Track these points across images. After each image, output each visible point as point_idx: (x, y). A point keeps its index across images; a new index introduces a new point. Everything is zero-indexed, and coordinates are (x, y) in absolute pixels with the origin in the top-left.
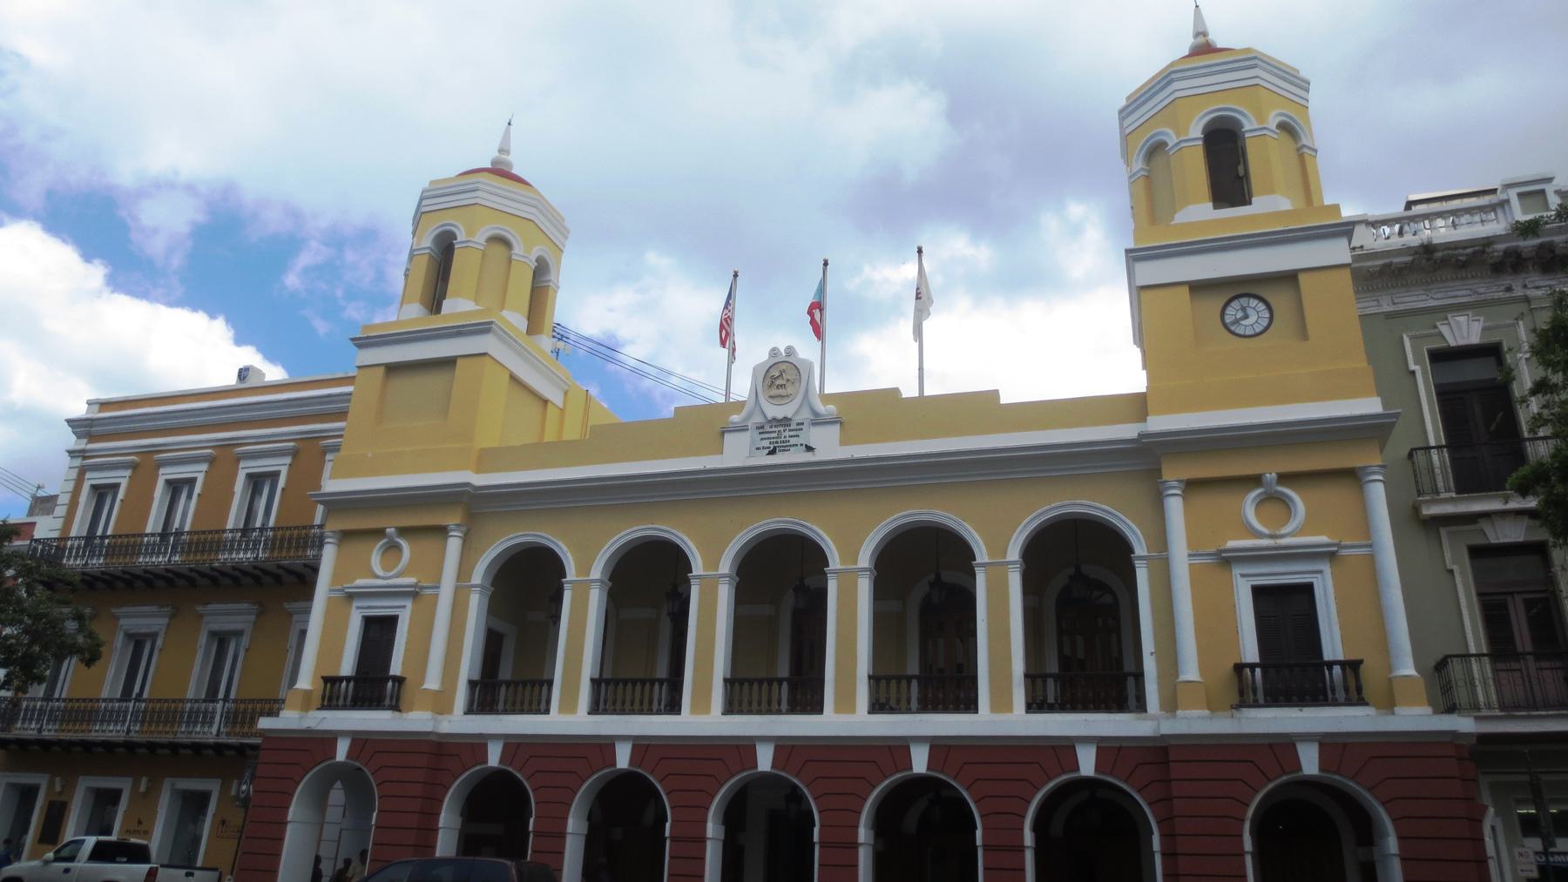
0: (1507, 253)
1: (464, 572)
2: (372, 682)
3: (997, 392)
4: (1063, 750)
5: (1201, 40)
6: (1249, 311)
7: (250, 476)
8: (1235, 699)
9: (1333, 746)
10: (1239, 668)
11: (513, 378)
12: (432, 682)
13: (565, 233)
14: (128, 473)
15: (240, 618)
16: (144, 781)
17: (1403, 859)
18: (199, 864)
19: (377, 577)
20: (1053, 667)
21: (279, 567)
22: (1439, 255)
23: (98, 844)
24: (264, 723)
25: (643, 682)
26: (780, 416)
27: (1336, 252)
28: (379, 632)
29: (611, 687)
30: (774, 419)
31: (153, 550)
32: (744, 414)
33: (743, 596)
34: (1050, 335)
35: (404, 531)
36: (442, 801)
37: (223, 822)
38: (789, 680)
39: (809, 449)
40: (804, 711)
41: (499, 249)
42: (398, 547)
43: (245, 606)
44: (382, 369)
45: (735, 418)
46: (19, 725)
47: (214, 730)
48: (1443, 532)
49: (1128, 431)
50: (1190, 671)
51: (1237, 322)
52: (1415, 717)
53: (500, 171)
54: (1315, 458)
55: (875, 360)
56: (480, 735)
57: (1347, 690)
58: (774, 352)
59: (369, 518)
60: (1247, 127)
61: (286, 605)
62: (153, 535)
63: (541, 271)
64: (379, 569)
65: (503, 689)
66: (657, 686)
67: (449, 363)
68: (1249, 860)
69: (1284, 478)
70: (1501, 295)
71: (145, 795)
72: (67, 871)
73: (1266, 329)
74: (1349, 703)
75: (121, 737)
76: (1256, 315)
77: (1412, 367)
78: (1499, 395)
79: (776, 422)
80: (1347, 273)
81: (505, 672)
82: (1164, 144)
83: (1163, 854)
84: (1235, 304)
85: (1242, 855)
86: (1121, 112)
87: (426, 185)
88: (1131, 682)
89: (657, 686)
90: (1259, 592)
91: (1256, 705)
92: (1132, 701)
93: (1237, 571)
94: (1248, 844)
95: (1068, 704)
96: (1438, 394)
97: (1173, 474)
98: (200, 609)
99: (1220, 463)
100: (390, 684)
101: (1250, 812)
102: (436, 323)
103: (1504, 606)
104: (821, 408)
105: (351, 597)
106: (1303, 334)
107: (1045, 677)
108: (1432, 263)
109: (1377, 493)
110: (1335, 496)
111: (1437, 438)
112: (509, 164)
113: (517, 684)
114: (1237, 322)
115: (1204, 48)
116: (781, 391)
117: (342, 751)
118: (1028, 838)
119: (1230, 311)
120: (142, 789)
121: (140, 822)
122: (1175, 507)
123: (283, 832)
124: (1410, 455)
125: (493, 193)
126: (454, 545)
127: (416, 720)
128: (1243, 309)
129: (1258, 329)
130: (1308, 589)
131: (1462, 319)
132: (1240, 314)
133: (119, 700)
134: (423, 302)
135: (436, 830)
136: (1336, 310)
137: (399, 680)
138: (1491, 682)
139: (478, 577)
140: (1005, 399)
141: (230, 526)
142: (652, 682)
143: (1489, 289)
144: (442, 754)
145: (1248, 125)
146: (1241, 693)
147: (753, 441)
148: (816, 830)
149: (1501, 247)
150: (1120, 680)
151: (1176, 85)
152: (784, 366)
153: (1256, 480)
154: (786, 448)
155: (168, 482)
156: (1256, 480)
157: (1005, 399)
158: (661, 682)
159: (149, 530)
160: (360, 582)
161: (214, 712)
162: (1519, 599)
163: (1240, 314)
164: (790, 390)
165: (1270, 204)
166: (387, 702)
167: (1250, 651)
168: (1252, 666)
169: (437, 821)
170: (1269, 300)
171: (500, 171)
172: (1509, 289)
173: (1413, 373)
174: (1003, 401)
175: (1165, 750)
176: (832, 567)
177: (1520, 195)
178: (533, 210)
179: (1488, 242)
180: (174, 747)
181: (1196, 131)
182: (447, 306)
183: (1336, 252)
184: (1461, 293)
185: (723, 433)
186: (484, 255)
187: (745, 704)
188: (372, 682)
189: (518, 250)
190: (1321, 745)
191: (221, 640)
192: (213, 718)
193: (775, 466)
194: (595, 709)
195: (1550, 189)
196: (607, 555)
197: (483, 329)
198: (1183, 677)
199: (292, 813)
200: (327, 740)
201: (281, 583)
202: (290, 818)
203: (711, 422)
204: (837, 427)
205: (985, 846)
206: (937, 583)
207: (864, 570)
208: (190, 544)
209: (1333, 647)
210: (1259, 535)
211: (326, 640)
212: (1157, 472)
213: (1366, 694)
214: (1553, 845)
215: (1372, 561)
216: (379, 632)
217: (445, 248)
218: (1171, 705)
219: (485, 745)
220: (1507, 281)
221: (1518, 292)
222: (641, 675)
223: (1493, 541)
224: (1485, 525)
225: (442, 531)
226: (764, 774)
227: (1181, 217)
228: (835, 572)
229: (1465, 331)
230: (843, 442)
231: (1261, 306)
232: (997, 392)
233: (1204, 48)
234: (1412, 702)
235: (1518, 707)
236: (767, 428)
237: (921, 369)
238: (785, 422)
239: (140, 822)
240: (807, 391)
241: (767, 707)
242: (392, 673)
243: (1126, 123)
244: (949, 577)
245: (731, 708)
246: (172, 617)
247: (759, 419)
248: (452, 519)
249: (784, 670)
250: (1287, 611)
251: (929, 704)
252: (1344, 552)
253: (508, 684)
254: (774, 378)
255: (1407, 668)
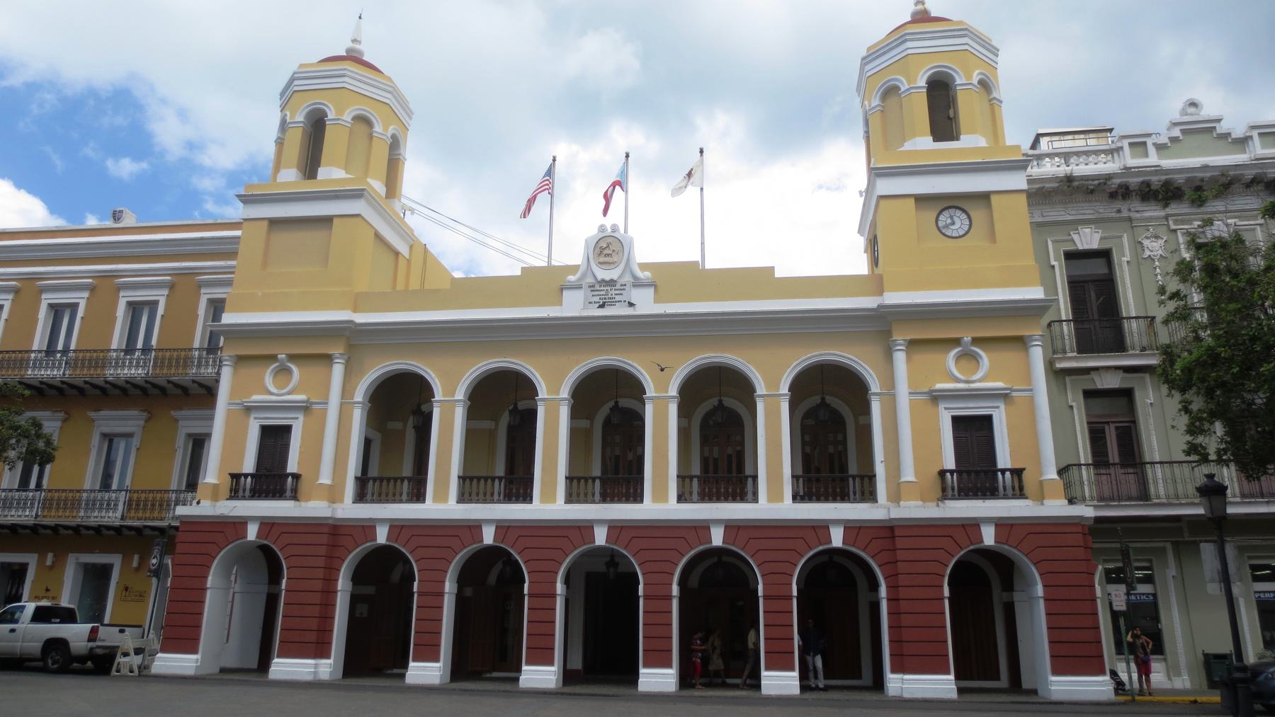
0: (1120, 186)
1: (346, 392)
2: (271, 477)
3: (773, 268)
4: (821, 528)
5: (920, 7)
6: (956, 219)
7: (130, 304)
8: (940, 494)
9: (1004, 526)
10: (942, 473)
11: (377, 235)
12: (325, 479)
13: (410, 114)
14: (10, 297)
15: (131, 423)
16: (50, 557)
17: (1046, 600)
18: (106, 621)
19: (272, 394)
20: (696, 470)
21: (169, 382)
22: (1076, 184)
23: (38, 609)
24: (181, 511)
25: (486, 479)
26: (607, 279)
27: (1017, 181)
28: (275, 438)
29: (377, 483)
30: (603, 280)
31: (38, 364)
32: (578, 275)
33: (575, 414)
34: (789, 220)
35: (292, 358)
36: (339, 570)
37: (126, 589)
38: (600, 478)
39: (631, 305)
40: (517, 501)
41: (362, 128)
42: (289, 371)
43: (135, 413)
44: (266, 223)
45: (572, 278)
46: (82, 514)
47: (119, 514)
48: (1068, 379)
49: (869, 302)
50: (908, 475)
51: (947, 226)
52: (1056, 507)
53: (353, 57)
54: (997, 327)
55: (662, 232)
56: (370, 519)
57: (1013, 488)
58: (602, 228)
59: (263, 347)
60: (958, 81)
61: (173, 413)
62: (40, 351)
63: (395, 145)
64: (275, 390)
65: (371, 482)
66: (497, 482)
67: (326, 221)
68: (947, 602)
69: (977, 341)
70: (1113, 215)
71: (51, 568)
72: (13, 631)
73: (967, 233)
74: (1014, 497)
75: (31, 522)
76: (959, 223)
77: (1053, 263)
78: (1107, 285)
79: (604, 282)
80: (1023, 197)
81: (373, 472)
82: (898, 88)
83: (889, 600)
84: (946, 213)
85: (942, 599)
86: (863, 59)
87: (295, 68)
88: (750, 481)
89: (497, 482)
90: (956, 420)
91: (953, 498)
92: (750, 495)
93: (942, 406)
94: (946, 592)
95: (707, 496)
96: (1069, 283)
97: (900, 337)
98: (92, 414)
99: (935, 329)
100: (290, 479)
101: (948, 572)
102: (309, 186)
103: (1103, 431)
104: (640, 274)
105: (249, 410)
106: (992, 236)
107: (691, 478)
108: (1072, 189)
109: (1037, 355)
110: (1009, 357)
111: (1067, 314)
112: (361, 53)
113: (381, 479)
114: (947, 226)
115: (922, 17)
116: (607, 259)
117: (252, 532)
118: (675, 590)
119: (941, 217)
120: (49, 563)
121: (47, 590)
122: (900, 358)
123: (204, 596)
124: (1049, 325)
125: (353, 78)
126: (338, 370)
127: (312, 508)
128: (951, 217)
129: (961, 233)
130: (989, 419)
131: (1087, 230)
132: (949, 221)
133: (18, 490)
134: (299, 169)
135: (335, 592)
136: (1014, 218)
137: (296, 477)
138: (1151, 481)
139: (359, 396)
140: (778, 274)
141: (114, 346)
142: (493, 479)
143: (1106, 209)
144: (336, 534)
145: (959, 80)
146: (944, 490)
147: (586, 298)
148: (641, 587)
149: (1117, 181)
150: (742, 480)
151: (909, 44)
152: (610, 240)
153: (956, 342)
154: (613, 303)
155: (51, 306)
156: (956, 342)
157: (778, 274)
158: (500, 479)
159: (35, 347)
160: (255, 397)
161: (117, 500)
162: (1112, 426)
163: (949, 221)
164: (615, 258)
165: (971, 141)
166: (288, 493)
167: (950, 462)
168: (952, 472)
169: (336, 586)
170: (972, 214)
171: (353, 57)
172: (1119, 211)
173: (1053, 267)
174: (777, 275)
175: (892, 529)
176: (648, 395)
177: (1131, 144)
178: (389, 95)
179: (1109, 177)
180: (77, 529)
181: (922, 82)
182: (322, 173)
183: (1017, 181)
184: (1088, 210)
185: (562, 290)
186: (351, 132)
187: (582, 495)
188: (271, 477)
189: (378, 128)
190: (996, 525)
191: (110, 438)
192: (116, 505)
193: (606, 317)
194: (461, 500)
195: (1150, 142)
196: (468, 382)
197: (357, 194)
198: (903, 479)
199: (210, 581)
200: (239, 525)
201: (176, 396)
202: (209, 585)
203: (548, 281)
204: (652, 290)
205: (765, 597)
206: (514, 412)
207: (673, 397)
208: (76, 360)
209: (1004, 459)
210: (958, 380)
211: (230, 445)
212: (888, 333)
213: (1027, 490)
214: (1134, 589)
215: (1031, 400)
216: (275, 438)
217: (317, 126)
218: (895, 497)
219: (374, 527)
220: (1118, 204)
221: (1125, 214)
222: (582, 475)
223: (1099, 387)
224: (1094, 375)
225: (328, 359)
226: (600, 548)
227: (908, 146)
228: (650, 398)
229: (1088, 239)
230: (656, 301)
231: (964, 216)
232: (773, 268)
233: (922, 17)
234: (1053, 497)
235: (1112, 499)
236: (597, 287)
237: (703, 243)
238: (612, 283)
239: (47, 590)
240: (628, 260)
241: (487, 498)
242: (289, 471)
243: (867, 68)
244: (522, 405)
245: (570, 499)
246: (64, 421)
247: (590, 280)
248: (337, 350)
249: (500, 470)
250: (974, 432)
251: (607, 497)
252: (1014, 394)
253: (375, 480)
254: (602, 249)
255: (1052, 474)
